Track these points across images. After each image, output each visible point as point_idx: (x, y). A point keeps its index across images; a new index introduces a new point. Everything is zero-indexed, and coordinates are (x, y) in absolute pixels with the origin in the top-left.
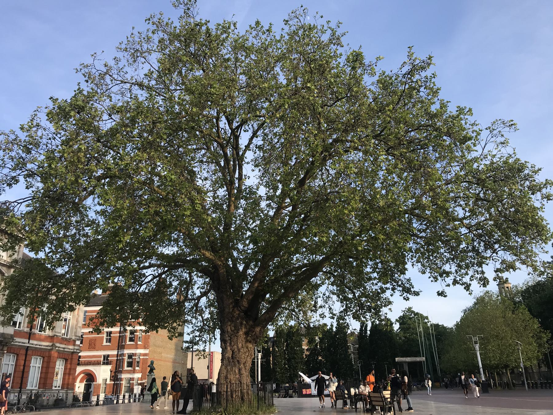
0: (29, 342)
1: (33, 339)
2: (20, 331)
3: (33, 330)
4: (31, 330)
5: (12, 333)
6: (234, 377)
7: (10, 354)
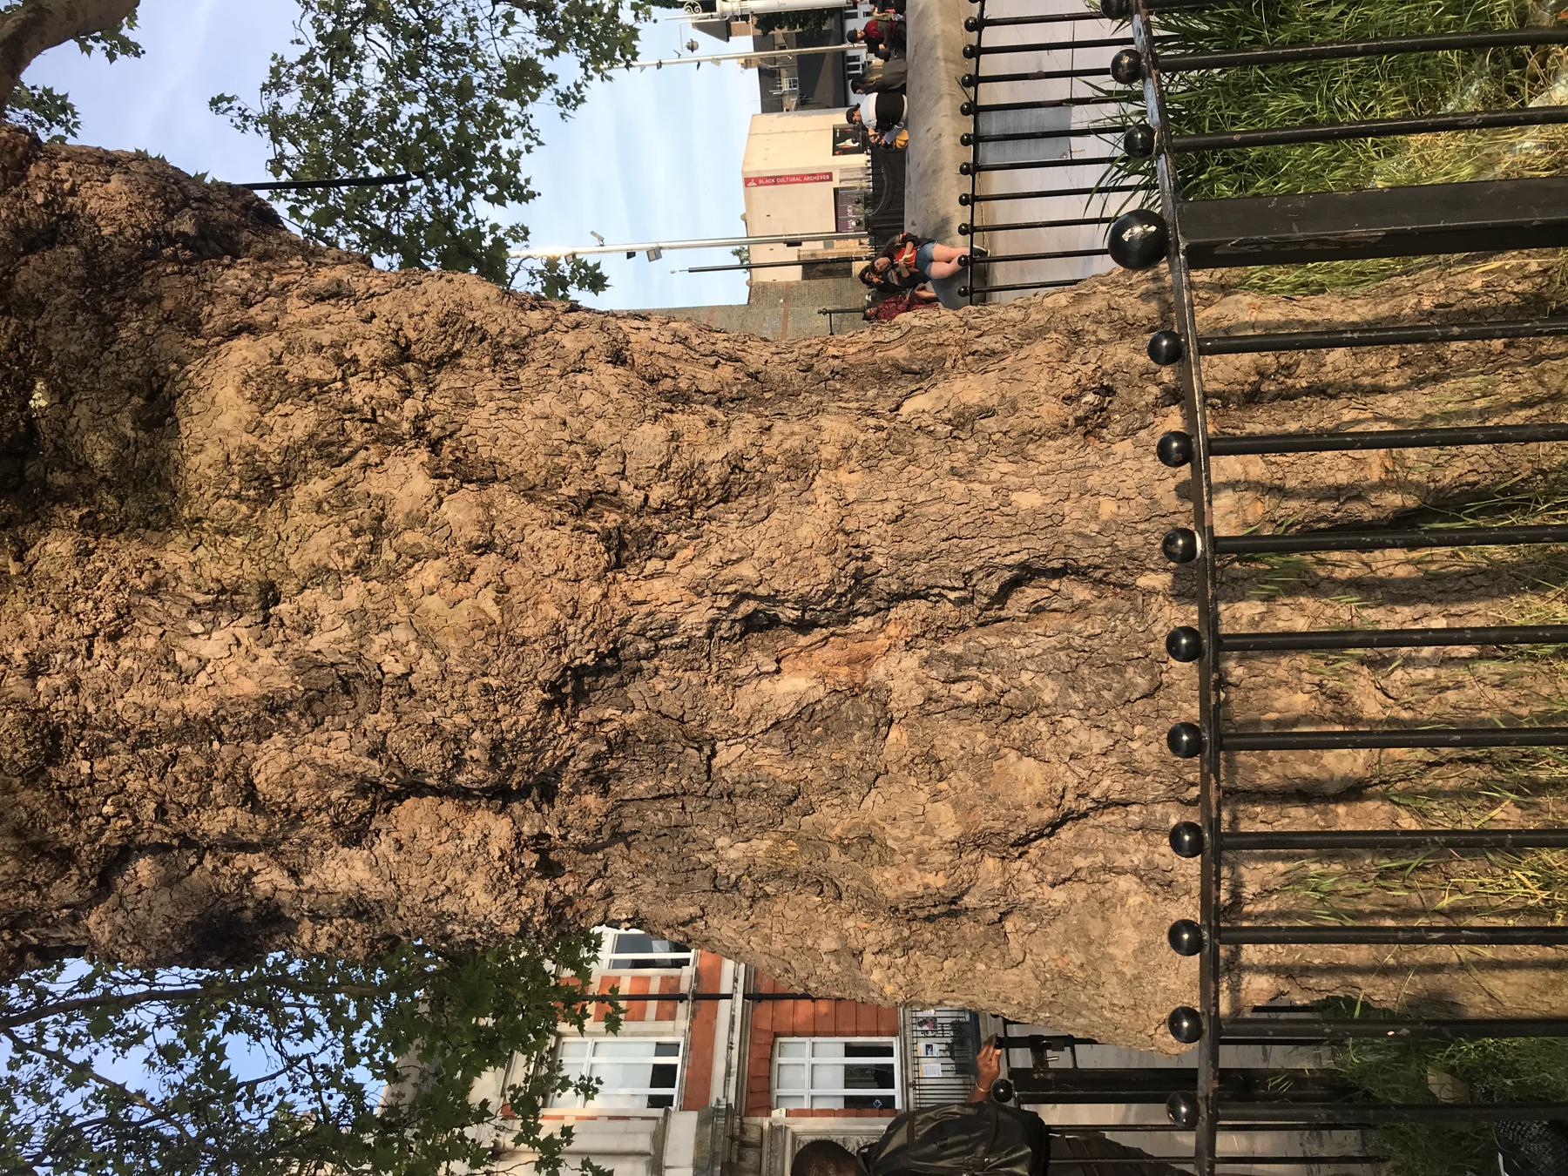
0: (729, 997)
1: (717, 981)
2: (691, 1046)
3: (684, 988)
4: (682, 998)
5: (692, 1118)
6: (931, 762)
7: (775, 1067)
